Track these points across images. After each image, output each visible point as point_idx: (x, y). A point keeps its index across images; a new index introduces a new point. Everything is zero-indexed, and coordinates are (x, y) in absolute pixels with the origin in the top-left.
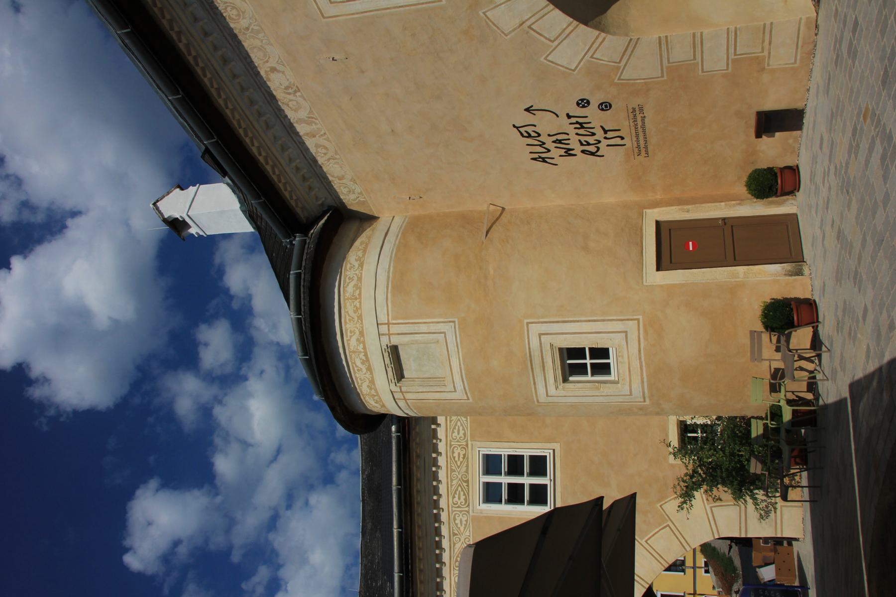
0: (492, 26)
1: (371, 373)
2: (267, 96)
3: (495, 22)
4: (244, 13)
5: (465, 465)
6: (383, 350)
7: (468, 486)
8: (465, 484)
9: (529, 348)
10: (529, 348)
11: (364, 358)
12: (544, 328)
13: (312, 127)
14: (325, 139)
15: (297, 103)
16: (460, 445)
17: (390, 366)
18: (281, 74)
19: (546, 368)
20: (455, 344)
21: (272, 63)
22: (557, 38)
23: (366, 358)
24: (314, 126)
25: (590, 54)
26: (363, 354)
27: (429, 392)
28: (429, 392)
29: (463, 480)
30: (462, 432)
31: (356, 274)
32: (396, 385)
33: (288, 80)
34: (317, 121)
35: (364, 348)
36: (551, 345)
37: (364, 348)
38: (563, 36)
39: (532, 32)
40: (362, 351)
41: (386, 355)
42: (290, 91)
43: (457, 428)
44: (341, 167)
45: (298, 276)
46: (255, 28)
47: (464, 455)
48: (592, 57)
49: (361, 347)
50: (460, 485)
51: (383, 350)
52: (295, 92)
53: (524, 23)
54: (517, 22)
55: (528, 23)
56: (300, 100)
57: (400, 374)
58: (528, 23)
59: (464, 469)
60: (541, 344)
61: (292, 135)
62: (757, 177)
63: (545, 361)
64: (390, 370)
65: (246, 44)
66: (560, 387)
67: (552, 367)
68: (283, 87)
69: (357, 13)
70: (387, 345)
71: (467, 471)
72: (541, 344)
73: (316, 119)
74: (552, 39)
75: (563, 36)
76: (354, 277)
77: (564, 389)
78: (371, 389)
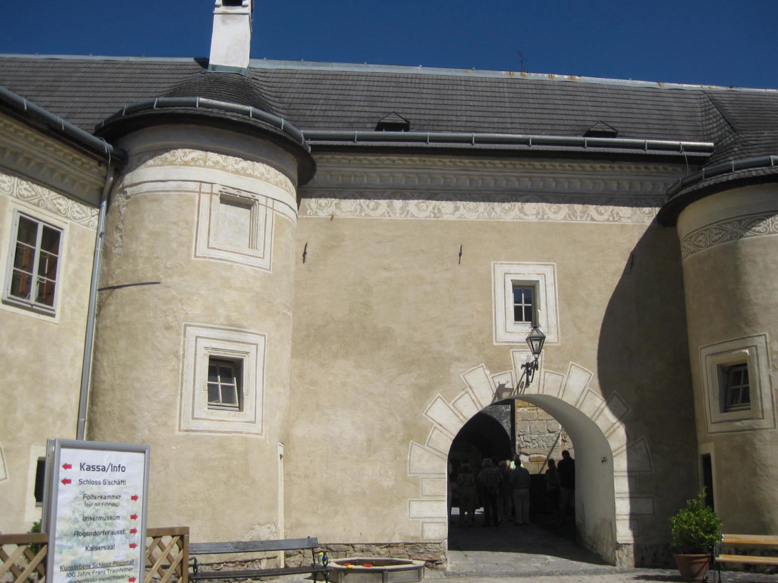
0: (472, 369)
1: (233, 172)
2: (435, 191)
3: (474, 372)
4: (505, 213)
5: (53, 208)
6: (254, 195)
7: (34, 204)
8: (36, 201)
9: (248, 332)
10: (248, 332)
11: (248, 172)
12: (261, 348)
13: (398, 209)
14: (384, 213)
15: (424, 210)
16: (68, 208)
17: (238, 194)
18: (452, 211)
19: (227, 343)
20: (254, 264)
21: (462, 211)
22: (456, 408)
23: (248, 174)
24: (398, 211)
25: (439, 427)
26: (252, 173)
27: (210, 220)
28: (210, 220)
29: (40, 200)
30: (76, 215)
31: (229, 165)
32: (220, 191)
33: (446, 214)
34: (403, 216)
35: (256, 177)
36: (247, 353)
37: (256, 177)
38: (457, 412)
39: (463, 392)
40: (255, 174)
41: (250, 195)
42: (436, 211)
43: (81, 212)
44: (351, 212)
45: (247, 113)
46: (493, 215)
47: (59, 210)
48: (435, 428)
49: (256, 173)
50: (52, 200)
51: (254, 195)
52: (434, 214)
53: (471, 389)
54: (473, 385)
55: (470, 392)
56: (427, 213)
57: (227, 200)
58: (470, 392)
59: (49, 206)
60: (250, 344)
61: (392, 191)
62: (29, 546)
63: (234, 343)
64: (235, 192)
65: (482, 203)
66: (206, 352)
67: (227, 349)
68: (440, 207)
69: (495, 287)
70: (258, 200)
71: (47, 208)
72: (250, 344)
73: (405, 216)
74: (455, 404)
75: (457, 412)
76: (227, 162)
77: (205, 355)
78: (214, 162)
